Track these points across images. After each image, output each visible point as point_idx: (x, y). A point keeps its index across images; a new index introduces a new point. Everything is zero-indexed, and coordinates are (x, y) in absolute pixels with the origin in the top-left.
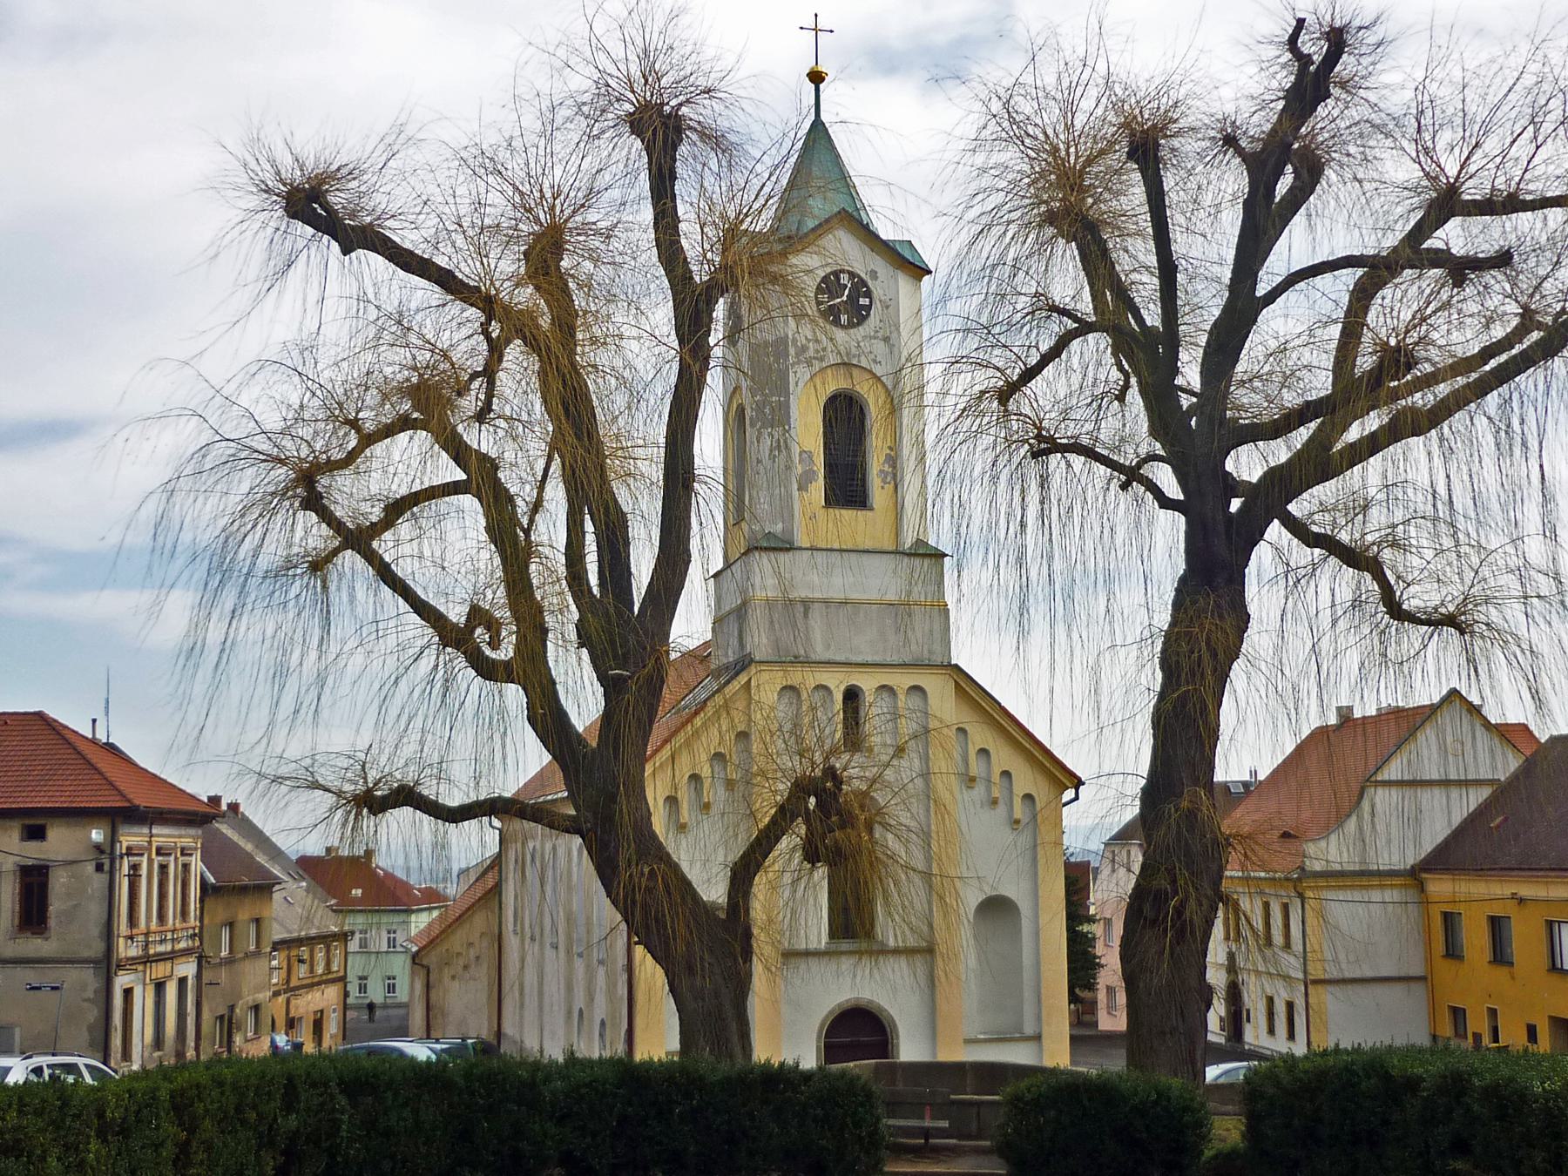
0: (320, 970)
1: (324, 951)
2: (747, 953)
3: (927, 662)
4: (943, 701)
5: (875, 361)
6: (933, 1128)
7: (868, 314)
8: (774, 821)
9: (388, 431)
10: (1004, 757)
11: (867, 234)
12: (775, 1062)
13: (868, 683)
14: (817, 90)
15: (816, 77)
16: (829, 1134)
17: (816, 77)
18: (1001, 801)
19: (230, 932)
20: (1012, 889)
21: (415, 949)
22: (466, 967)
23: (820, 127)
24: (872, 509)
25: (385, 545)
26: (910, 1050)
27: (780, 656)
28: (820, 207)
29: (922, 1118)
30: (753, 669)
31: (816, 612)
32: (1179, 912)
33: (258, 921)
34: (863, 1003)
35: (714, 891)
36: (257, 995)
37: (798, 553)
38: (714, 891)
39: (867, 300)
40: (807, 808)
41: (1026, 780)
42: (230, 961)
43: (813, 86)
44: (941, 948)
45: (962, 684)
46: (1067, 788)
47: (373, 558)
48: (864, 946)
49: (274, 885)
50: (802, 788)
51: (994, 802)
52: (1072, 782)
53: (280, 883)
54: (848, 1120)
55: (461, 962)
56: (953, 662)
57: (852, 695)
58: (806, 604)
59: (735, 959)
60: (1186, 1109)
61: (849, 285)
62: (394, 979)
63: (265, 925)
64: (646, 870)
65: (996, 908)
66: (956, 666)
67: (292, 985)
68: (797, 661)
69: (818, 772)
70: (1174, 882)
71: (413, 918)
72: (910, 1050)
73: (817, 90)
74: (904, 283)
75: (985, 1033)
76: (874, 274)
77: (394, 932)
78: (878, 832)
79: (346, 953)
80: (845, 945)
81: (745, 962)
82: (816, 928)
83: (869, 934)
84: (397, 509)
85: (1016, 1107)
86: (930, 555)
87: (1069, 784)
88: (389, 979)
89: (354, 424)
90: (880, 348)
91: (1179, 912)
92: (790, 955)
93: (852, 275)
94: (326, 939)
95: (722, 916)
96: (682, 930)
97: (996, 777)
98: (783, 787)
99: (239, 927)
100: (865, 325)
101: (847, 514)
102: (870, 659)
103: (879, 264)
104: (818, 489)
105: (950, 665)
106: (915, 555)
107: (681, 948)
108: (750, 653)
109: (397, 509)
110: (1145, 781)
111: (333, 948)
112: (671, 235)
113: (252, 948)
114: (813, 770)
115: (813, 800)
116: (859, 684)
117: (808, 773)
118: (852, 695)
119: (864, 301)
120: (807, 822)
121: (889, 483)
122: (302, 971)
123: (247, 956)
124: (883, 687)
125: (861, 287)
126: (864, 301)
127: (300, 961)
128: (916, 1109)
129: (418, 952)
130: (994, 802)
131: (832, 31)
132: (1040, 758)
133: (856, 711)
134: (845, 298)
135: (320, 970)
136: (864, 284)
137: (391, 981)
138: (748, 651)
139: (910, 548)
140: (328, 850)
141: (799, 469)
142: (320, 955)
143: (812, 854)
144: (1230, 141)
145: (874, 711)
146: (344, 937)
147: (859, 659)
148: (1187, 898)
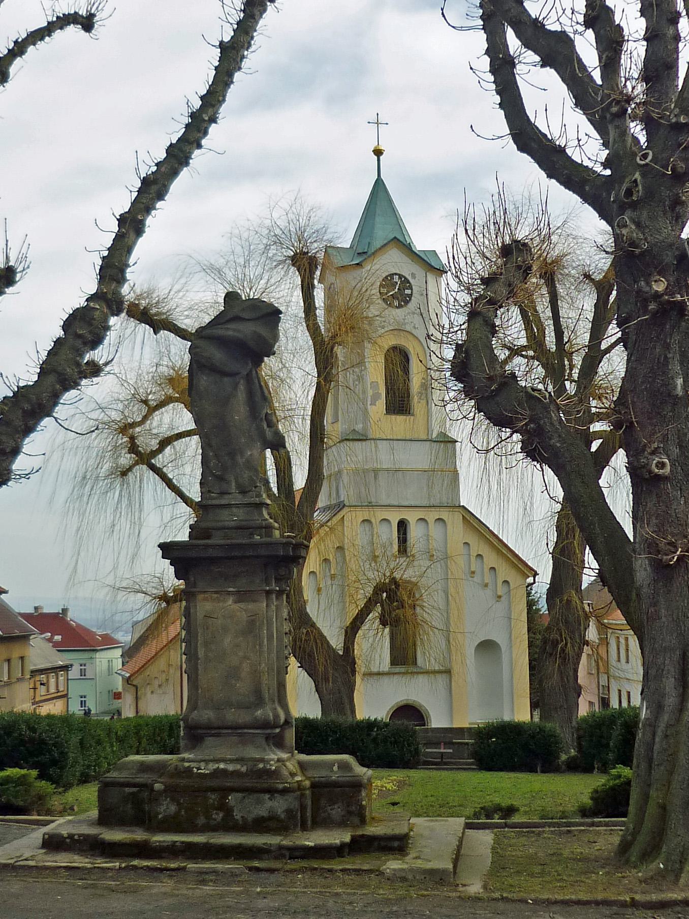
0: (52, 689)
1: (55, 677)
2: (354, 672)
3: (446, 505)
4: (456, 530)
5: (415, 328)
6: (445, 752)
7: (410, 299)
8: (366, 606)
9: (161, 404)
10: (491, 559)
11: (407, 248)
12: (372, 718)
13: (412, 517)
14: (379, 160)
15: (378, 153)
16: (397, 749)
17: (378, 153)
18: (490, 586)
19: (8, 666)
20: (500, 638)
21: (128, 675)
22: (160, 686)
23: (380, 182)
24: (413, 415)
25: (158, 461)
26: (437, 721)
27: (361, 502)
28: (381, 234)
29: (440, 748)
30: (346, 510)
31: (383, 479)
32: (563, 650)
33: (22, 658)
34: (410, 702)
35: (336, 641)
36: (23, 706)
37: (368, 442)
38: (336, 641)
39: (410, 291)
40: (382, 599)
41: (505, 572)
42: (8, 684)
43: (376, 157)
44: (456, 669)
45: (466, 516)
46: (529, 577)
47: (153, 468)
48: (411, 669)
49: (30, 635)
50: (378, 589)
51: (486, 585)
52: (531, 573)
53: (34, 634)
54: (406, 743)
55: (157, 683)
56: (461, 504)
57: (402, 525)
58: (376, 471)
59: (348, 674)
60: (552, 736)
61: (399, 283)
62: (85, 697)
63: (26, 661)
64: (305, 631)
65: (487, 647)
66: (463, 506)
67: (37, 700)
68: (370, 505)
69: (387, 581)
70: (561, 636)
71: (98, 655)
72: (437, 721)
73: (379, 160)
74: (431, 279)
75: (481, 720)
76: (413, 276)
77: (85, 665)
78: (418, 609)
79: (68, 680)
80: (397, 669)
81: (353, 676)
82: (382, 658)
83: (415, 663)
84: (166, 442)
85: (480, 736)
86: (449, 442)
87: (529, 575)
88: (81, 698)
89: (145, 402)
90: (417, 320)
91: (563, 650)
92: (370, 674)
93: (400, 276)
94: (56, 669)
95: (341, 653)
96: (322, 660)
97: (486, 570)
98: (370, 590)
99: (13, 663)
100: (410, 305)
101: (400, 418)
102: (413, 504)
103: (419, 272)
104: (381, 404)
105: (460, 506)
106: (437, 441)
107: (321, 669)
108: (344, 501)
109: (166, 442)
110: (549, 586)
111: (60, 675)
112: (314, 320)
113: (6, 679)
114: (385, 580)
115: (385, 595)
116: (409, 520)
117: (382, 581)
118: (402, 525)
119: (408, 292)
120: (382, 606)
121: (423, 399)
122: (42, 690)
123: (19, 680)
124: (421, 519)
125: (406, 283)
126: (408, 292)
127: (41, 684)
128: (437, 744)
129: (130, 677)
130: (486, 585)
131: (387, 124)
132: (512, 559)
133: (405, 533)
134: (396, 290)
135: (52, 689)
136: (408, 282)
137: (83, 699)
138: (342, 500)
139: (435, 438)
140: (36, 608)
141: (370, 392)
142: (52, 681)
143: (384, 623)
144: (587, 276)
145: (415, 533)
146: (66, 668)
147: (406, 504)
148: (566, 644)
